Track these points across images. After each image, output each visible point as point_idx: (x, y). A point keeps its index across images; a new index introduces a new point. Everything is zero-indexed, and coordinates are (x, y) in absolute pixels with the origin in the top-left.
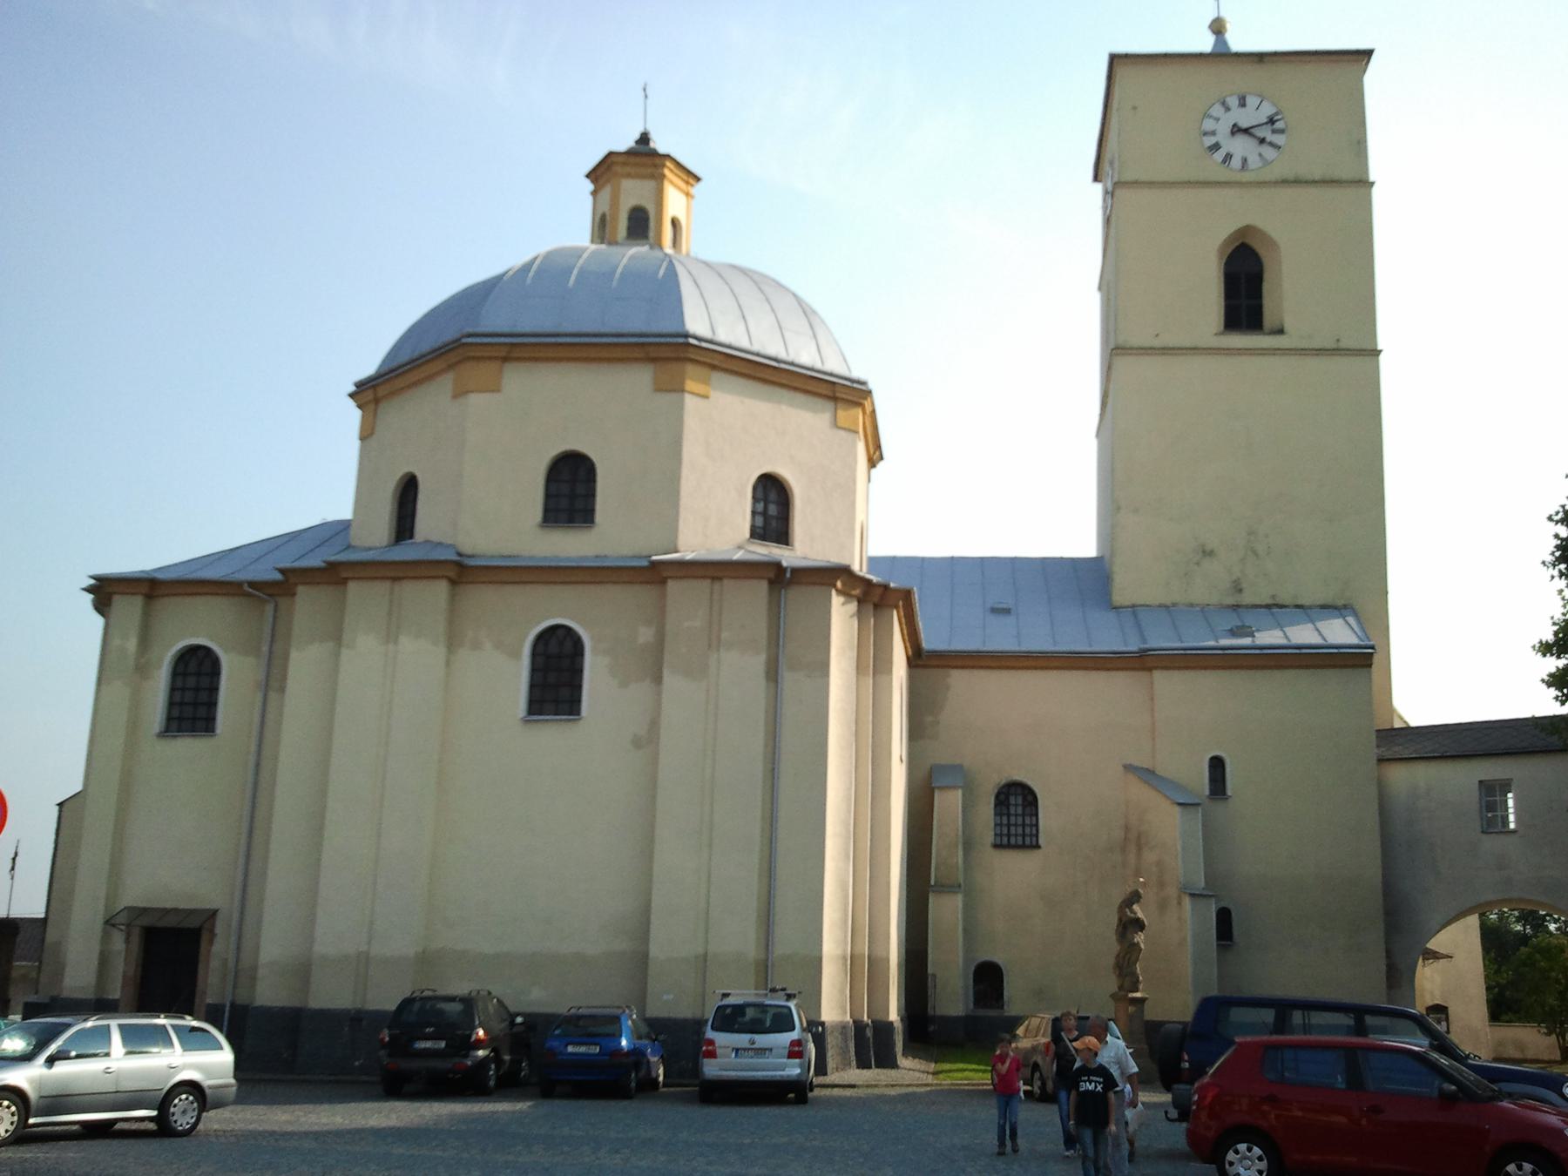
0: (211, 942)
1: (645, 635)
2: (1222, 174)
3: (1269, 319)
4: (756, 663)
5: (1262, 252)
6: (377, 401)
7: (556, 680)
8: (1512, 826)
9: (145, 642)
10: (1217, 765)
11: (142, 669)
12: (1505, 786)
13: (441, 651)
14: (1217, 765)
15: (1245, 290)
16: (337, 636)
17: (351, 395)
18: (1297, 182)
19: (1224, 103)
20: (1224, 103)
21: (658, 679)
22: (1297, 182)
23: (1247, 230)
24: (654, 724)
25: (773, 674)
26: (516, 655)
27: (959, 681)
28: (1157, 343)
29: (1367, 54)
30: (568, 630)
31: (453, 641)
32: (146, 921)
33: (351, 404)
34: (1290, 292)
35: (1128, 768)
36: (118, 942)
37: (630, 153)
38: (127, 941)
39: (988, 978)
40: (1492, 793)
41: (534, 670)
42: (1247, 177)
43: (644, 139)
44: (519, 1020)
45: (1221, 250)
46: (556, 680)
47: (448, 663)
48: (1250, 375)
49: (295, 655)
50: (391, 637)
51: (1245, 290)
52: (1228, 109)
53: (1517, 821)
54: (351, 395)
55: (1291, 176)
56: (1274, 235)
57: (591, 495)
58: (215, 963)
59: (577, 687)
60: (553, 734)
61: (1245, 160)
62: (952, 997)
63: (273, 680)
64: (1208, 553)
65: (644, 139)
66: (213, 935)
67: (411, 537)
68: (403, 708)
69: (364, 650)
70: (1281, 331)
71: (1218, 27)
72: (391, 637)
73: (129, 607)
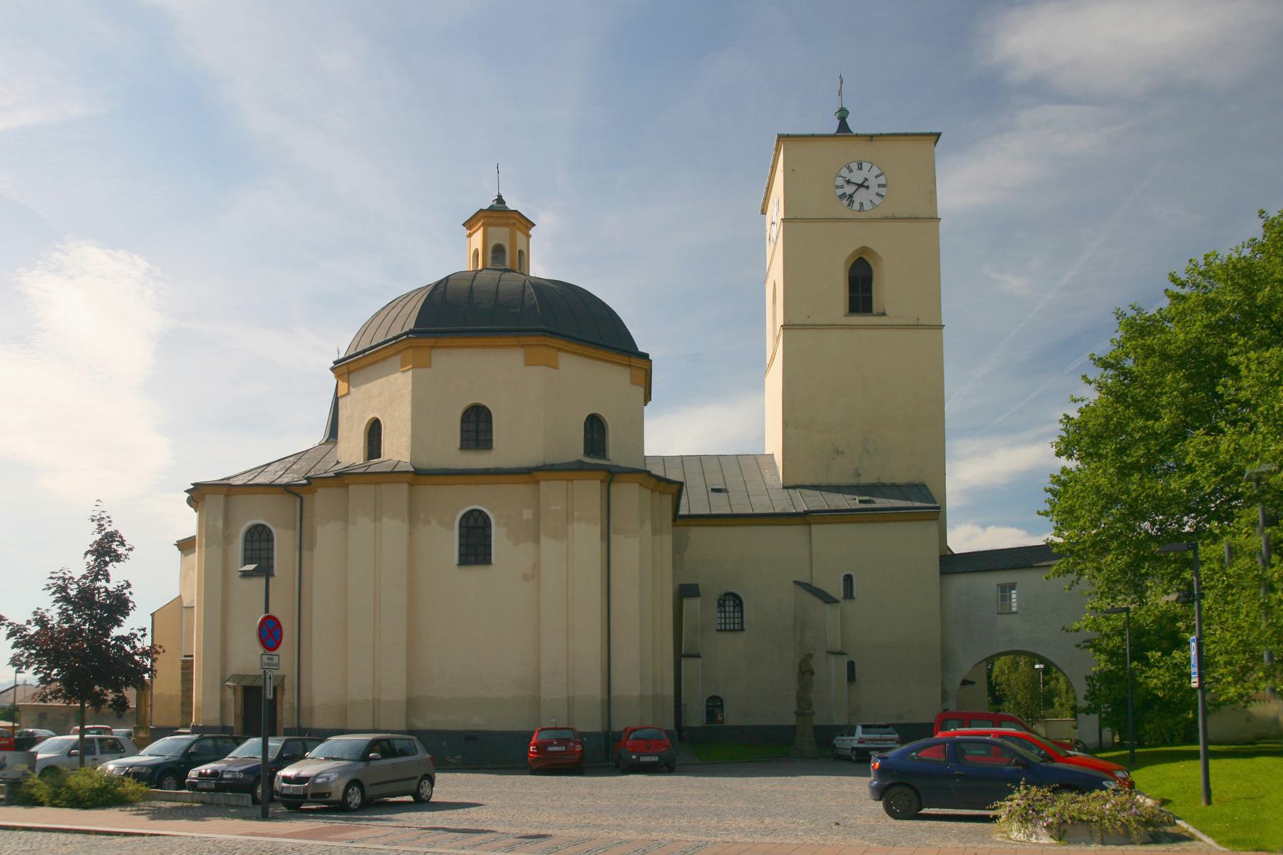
0: (283, 694)
1: (528, 514)
2: (848, 214)
3: (875, 308)
4: (596, 531)
5: (871, 263)
6: (349, 373)
7: (475, 543)
8: (1014, 609)
9: (227, 523)
10: (848, 579)
11: (227, 539)
12: (1013, 586)
13: (405, 526)
14: (848, 579)
15: (861, 288)
16: (345, 519)
17: (332, 369)
18: (894, 218)
19: (884, 186)
20: (884, 186)
21: (537, 541)
22: (894, 218)
23: (864, 249)
24: (536, 567)
25: (607, 537)
26: (453, 529)
27: (697, 534)
28: (808, 322)
29: (938, 135)
30: (480, 512)
31: (412, 519)
32: (247, 683)
33: (332, 374)
34: (885, 290)
35: (796, 583)
36: (230, 695)
37: (491, 209)
38: (235, 694)
39: (714, 705)
40: (1005, 589)
41: (461, 536)
42: (862, 215)
43: (500, 200)
44: (146, 676)
45: (846, 263)
46: (475, 543)
47: (410, 533)
48: (862, 339)
49: (319, 529)
50: (377, 518)
51: (861, 288)
52: (879, 186)
53: (1019, 606)
54: (332, 369)
55: (890, 215)
56: (880, 253)
57: (489, 430)
58: (286, 706)
59: (488, 546)
60: (474, 574)
61: (861, 204)
62: (696, 717)
63: (303, 544)
64: (839, 452)
65: (500, 200)
66: (283, 690)
67: (379, 456)
68: (837, 668)
69: (363, 525)
70: (884, 314)
71: (843, 115)
72: (377, 518)
73: (216, 502)
